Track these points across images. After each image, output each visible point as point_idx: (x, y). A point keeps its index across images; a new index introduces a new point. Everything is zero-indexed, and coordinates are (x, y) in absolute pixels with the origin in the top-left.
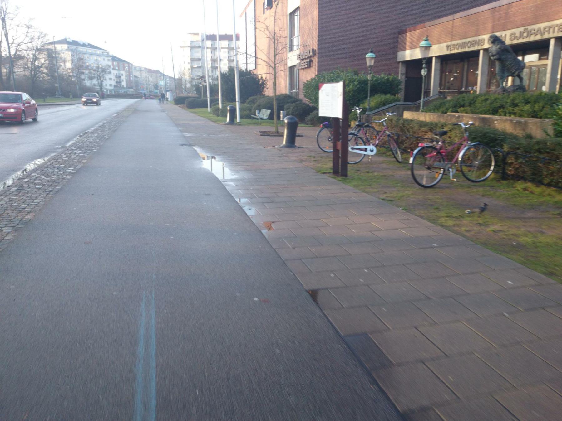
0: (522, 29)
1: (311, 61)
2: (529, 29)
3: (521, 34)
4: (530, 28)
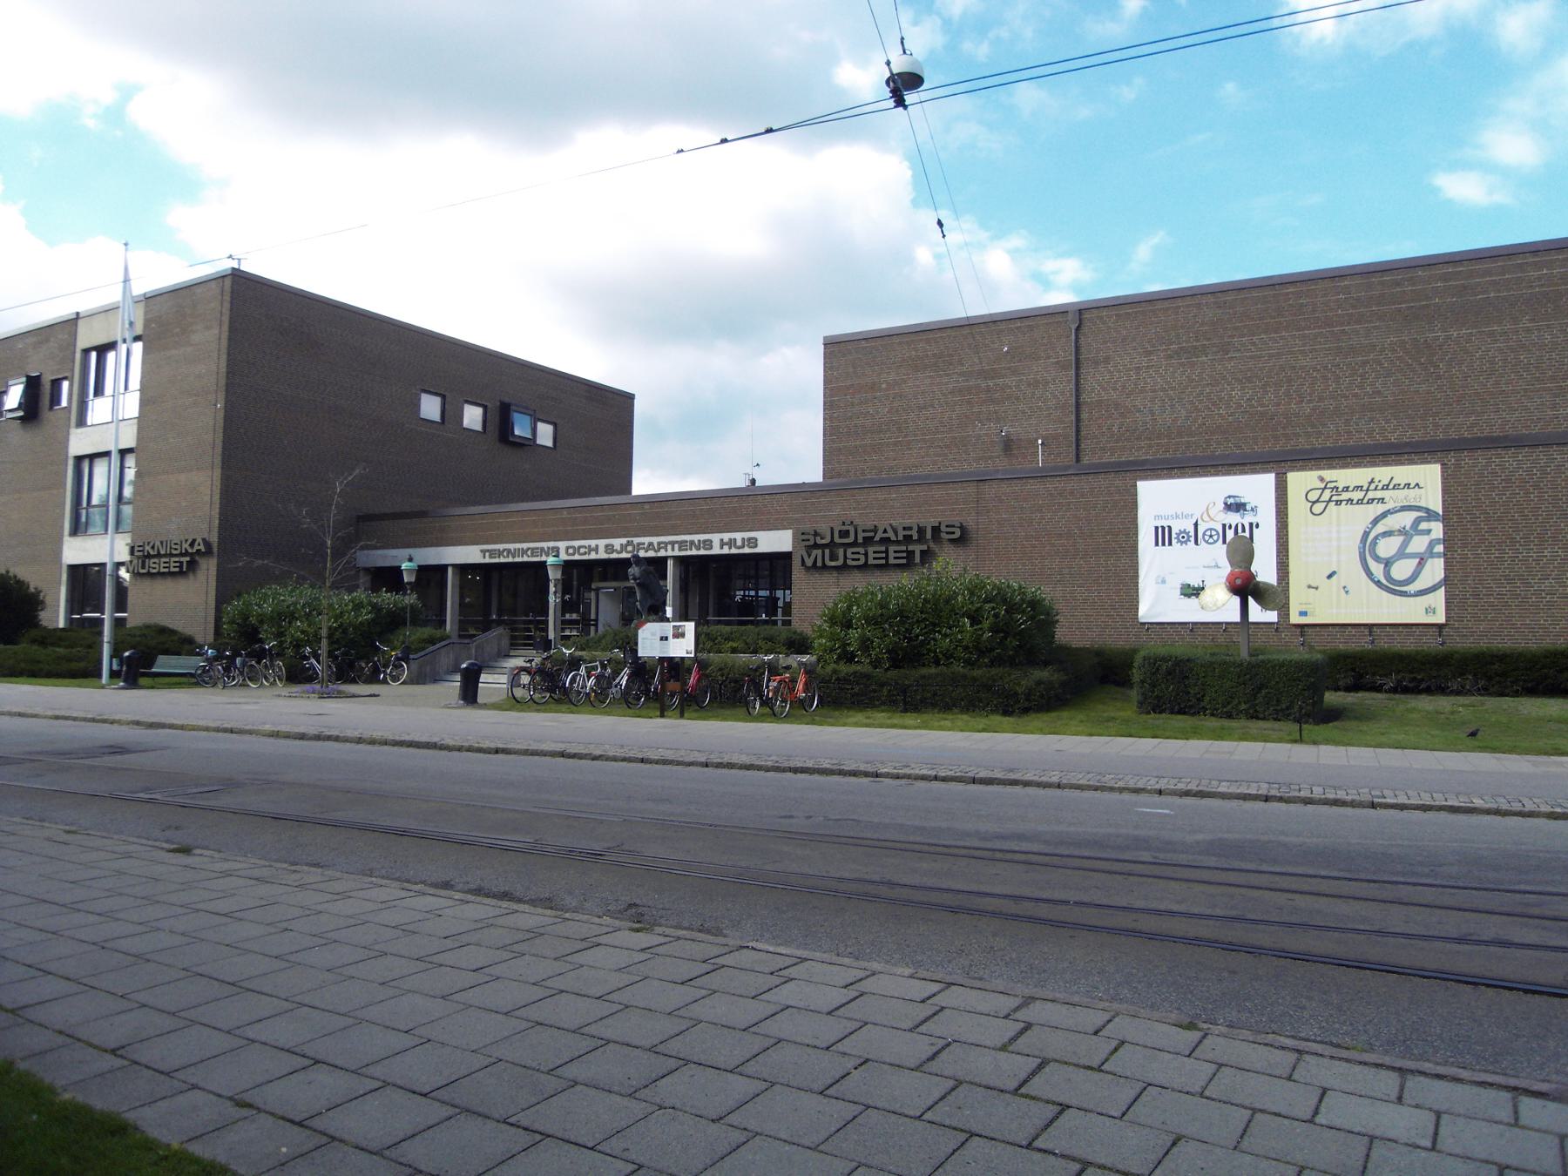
0: (624, 541)
1: (193, 565)
2: (635, 543)
3: (623, 548)
4: (636, 540)
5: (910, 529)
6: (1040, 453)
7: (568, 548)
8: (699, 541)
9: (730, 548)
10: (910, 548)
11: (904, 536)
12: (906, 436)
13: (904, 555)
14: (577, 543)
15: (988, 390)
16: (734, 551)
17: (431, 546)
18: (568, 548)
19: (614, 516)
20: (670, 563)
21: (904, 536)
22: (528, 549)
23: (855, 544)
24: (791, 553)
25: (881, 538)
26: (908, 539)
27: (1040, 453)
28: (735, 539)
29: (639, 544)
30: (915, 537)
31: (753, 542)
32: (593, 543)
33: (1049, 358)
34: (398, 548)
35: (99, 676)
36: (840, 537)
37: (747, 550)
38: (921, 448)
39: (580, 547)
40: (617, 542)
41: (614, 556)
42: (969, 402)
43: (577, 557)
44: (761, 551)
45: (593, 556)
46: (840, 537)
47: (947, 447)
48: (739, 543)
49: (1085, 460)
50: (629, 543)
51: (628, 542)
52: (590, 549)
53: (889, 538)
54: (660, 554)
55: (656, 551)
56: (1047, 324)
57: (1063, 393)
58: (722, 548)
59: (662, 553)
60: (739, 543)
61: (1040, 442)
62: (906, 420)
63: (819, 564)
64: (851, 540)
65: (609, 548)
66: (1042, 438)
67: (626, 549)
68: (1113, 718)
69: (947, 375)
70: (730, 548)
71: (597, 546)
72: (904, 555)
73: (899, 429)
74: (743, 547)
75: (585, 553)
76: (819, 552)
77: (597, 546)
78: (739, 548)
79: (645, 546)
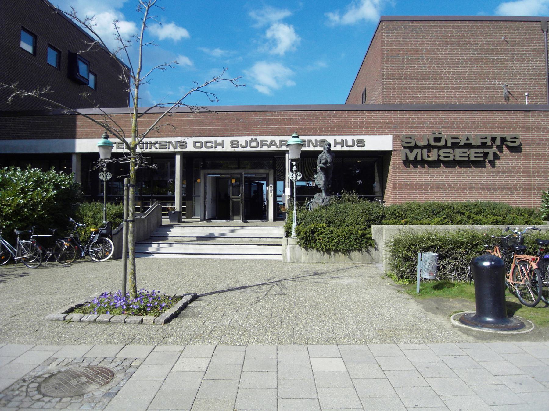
0: (249, 139)
5: (486, 138)
6: (526, 101)
7: (195, 143)
8: (316, 141)
9: (342, 147)
10: (486, 151)
11: (452, 143)
12: (440, 84)
13: (482, 155)
14: (203, 139)
15: (494, 61)
16: (345, 148)
17: (56, 138)
18: (195, 143)
19: (239, 120)
20: (178, 158)
21: (452, 143)
22: (157, 142)
23: (445, 147)
24: (392, 151)
25: (465, 143)
26: (484, 145)
27: (526, 101)
28: (346, 141)
29: (262, 141)
30: (489, 144)
31: (361, 143)
32: (219, 139)
33: (529, 46)
34: (20, 138)
35: (266, 218)
36: (435, 142)
37: (356, 148)
38: (450, 92)
39: (207, 142)
40: (242, 140)
41: (240, 149)
42: (481, 67)
43: (204, 149)
44: (189, 151)
45: (219, 149)
46: (435, 142)
47: (468, 92)
48: (350, 143)
49: (368, 102)
50: (252, 141)
51: (252, 139)
52: (217, 144)
53: (471, 144)
54: (281, 149)
55: (277, 147)
56: (528, 27)
57: (538, 67)
58: (335, 146)
59: (172, 150)
60: (350, 143)
61: (526, 94)
62: (440, 75)
63: (419, 159)
64: (442, 143)
65: (234, 144)
66: (529, 92)
67: (250, 144)
68: (432, 246)
69: (467, 49)
70: (342, 147)
71: (223, 142)
72: (482, 155)
73: (436, 79)
74: (353, 146)
75: (212, 147)
76: (419, 151)
77: (223, 142)
78: (350, 146)
79: (268, 143)
